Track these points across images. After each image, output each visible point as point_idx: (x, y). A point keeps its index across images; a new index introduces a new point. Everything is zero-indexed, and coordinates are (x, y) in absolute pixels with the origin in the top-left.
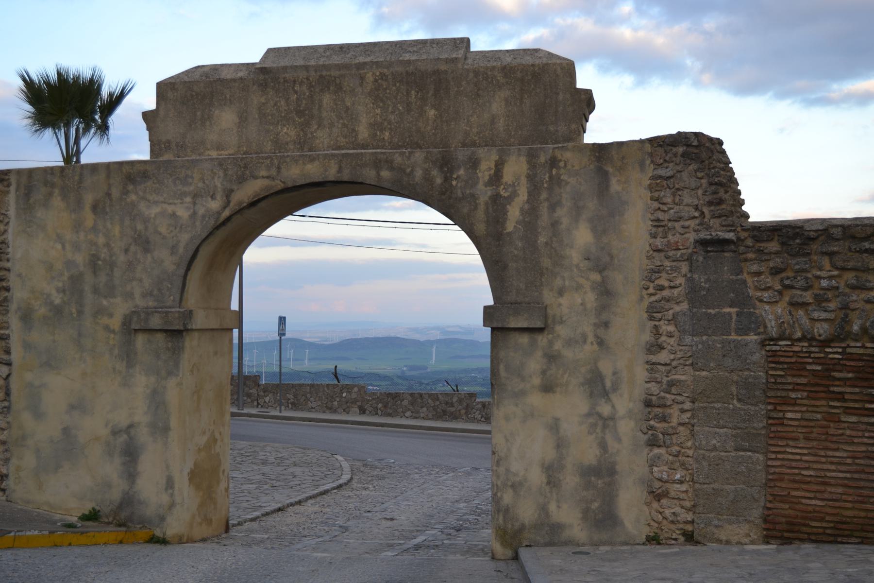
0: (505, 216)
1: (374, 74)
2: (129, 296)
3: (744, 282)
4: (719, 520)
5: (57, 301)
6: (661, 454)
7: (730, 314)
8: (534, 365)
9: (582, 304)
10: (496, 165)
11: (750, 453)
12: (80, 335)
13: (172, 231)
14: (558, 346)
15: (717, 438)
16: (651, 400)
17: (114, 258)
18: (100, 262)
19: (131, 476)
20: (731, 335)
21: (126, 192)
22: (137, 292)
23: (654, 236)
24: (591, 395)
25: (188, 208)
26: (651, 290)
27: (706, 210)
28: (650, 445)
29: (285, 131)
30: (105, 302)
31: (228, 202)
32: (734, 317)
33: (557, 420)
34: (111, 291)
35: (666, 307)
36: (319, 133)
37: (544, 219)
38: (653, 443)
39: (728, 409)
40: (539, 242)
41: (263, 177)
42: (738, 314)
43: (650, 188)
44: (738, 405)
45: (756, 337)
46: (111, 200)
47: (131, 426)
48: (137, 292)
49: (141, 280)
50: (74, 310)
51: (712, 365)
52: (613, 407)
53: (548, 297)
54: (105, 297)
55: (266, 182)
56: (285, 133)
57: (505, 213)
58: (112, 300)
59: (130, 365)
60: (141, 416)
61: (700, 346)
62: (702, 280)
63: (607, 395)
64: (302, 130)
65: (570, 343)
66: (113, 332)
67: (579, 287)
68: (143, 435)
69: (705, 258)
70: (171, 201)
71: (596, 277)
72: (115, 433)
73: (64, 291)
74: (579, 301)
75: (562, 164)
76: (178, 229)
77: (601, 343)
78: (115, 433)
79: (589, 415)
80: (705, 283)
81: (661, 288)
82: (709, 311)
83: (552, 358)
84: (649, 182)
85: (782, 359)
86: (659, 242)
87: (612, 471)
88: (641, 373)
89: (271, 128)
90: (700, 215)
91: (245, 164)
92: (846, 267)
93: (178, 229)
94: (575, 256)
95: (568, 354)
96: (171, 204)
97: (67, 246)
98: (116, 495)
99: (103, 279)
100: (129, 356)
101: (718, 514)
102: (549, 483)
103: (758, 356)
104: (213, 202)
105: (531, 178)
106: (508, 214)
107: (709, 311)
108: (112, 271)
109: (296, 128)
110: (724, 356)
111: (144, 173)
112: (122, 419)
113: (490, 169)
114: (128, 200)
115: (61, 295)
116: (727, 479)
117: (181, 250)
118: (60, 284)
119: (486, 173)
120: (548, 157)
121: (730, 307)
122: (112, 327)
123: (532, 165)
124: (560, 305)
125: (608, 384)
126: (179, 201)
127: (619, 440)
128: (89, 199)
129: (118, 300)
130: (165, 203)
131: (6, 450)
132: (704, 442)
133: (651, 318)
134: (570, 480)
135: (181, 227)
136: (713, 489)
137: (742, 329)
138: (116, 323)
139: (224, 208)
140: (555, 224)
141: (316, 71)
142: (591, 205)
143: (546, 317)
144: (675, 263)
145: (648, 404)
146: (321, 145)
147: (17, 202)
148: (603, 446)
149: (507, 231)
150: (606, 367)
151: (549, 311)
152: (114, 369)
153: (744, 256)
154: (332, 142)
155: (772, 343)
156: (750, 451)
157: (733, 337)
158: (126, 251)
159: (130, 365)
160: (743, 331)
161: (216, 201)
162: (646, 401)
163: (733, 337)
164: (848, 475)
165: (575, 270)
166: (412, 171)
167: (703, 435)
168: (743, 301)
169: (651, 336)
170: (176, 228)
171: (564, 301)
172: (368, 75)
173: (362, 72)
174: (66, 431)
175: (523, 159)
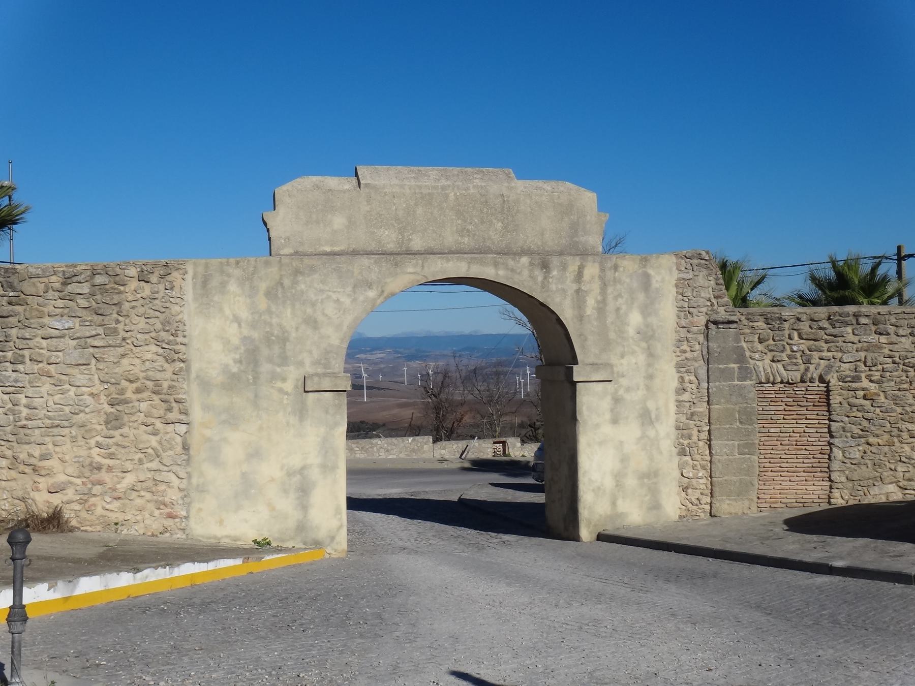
0: (585, 304)
1: (455, 194)
2: (301, 364)
3: (742, 348)
4: (729, 500)
5: (235, 370)
6: (687, 461)
7: (734, 368)
8: (606, 404)
9: (636, 363)
10: (579, 268)
11: (749, 456)
12: (256, 396)
13: (336, 314)
14: (621, 392)
15: (727, 448)
16: (679, 426)
17: (286, 334)
18: (273, 338)
19: (304, 507)
20: (735, 381)
21: (295, 283)
22: (308, 361)
23: (679, 317)
24: (643, 424)
25: (349, 295)
26: (678, 354)
27: (714, 301)
28: (680, 455)
29: (387, 233)
30: (278, 370)
31: (383, 292)
32: (736, 369)
33: (621, 443)
34: (284, 360)
35: (689, 364)
36: (414, 237)
37: (611, 306)
38: (682, 453)
39: (734, 428)
40: (607, 322)
41: (410, 273)
42: (739, 368)
43: (677, 286)
44: (740, 426)
45: (751, 382)
46: (283, 288)
47: (303, 468)
48: (308, 361)
49: (310, 352)
50: (250, 377)
51: (722, 400)
52: (657, 431)
53: (614, 360)
54: (279, 366)
55: (412, 277)
56: (386, 235)
57: (585, 302)
58: (285, 368)
59: (302, 418)
60: (314, 459)
61: (714, 389)
62: (715, 347)
63: (653, 424)
64: (400, 233)
65: (628, 390)
66: (287, 393)
67: (633, 352)
68: (315, 474)
69: (717, 332)
70: (335, 290)
71: (644, 345)
72: (290, 474)
73: (240, 362)
74: (634, 361)
75: (621, 269)
76: (341, 312)
77: (648, 388)
78: (290, 474)
79: (642, 438)
80: (717, 348)
81: (684, 352)
82: (720, 366)
83: (617, 400)
84: (675, 282)
85: (767, 396)
86: (683, 322)
87: (656, 474)
88: (673, 408)
89: (375, 230)
90: (711, 305)
91: (395, 263)
92: (18, 213)
93: (341, 312)
94: (631, 331)
95: (628, 397)
96: (335, 292)
97: (243, 325)
98: (291, 523)
99: (276, 349)
100: (301, 412)
101: (729, 496)
102: (617, 486)
103: (753, 394)
104: (371, 291)
105: (601, 278)
106: (587, 302)
107: (720, 366)
108: (285, 345)
109: (395, 231)
110: (731, 395)
111: (312, 267)
112: (296, 462)
113: (575, 271)
114: (299, 288)
115: (238, 365)
116: (735, 473)
117: (345, 328)
118: (237, 356)
119: (572, 274)
120: (613, 264)
121: (734, 364)
122: (286, 390)
123: (603, 270)
124: (622, 364)
125: (653, 416)
126: (342, 290)
127: (661, 453)
128: (263, 286)
129: (292, 368)
130: (330, 291)
131: (185, 496)
132: (718, 451)
133: (679, 372)
134: (631, 482)
135: (344, 311)
136: (725, 480)
137: (743, 377)
138: (289, 386)
139: (380, 296)
140: (618, 310)
141: (410, 189)
142: (641, 296)
143: (612, 373)
144: (695, 335)
145: (678, 428)
146: (415, 246)
147: (194, 288)
148: (651, 459)
149: (587, 314)
150: (651, 405)
151: (615, 369)
152: (288, 423)
153: (743, 331)
154: (424, 244)
155: (759, 386)
156: (749, 454)
157: (736, 382)
158: (297, 329)
159: (302, 418)
160: (742, 378)
161: (373, 291)
162: (676, 427)
163: (736, 382)
164: (810, 465)
165: (631, 341)
166: (521, 271)
167: (717, 446)
168: (741, 358)
169: (678, 384)
170: (339, 311)
171: (624, 361)
172: (451, 194)
173: (447, 192)
174: (244, 475)
175: (597, 265)
